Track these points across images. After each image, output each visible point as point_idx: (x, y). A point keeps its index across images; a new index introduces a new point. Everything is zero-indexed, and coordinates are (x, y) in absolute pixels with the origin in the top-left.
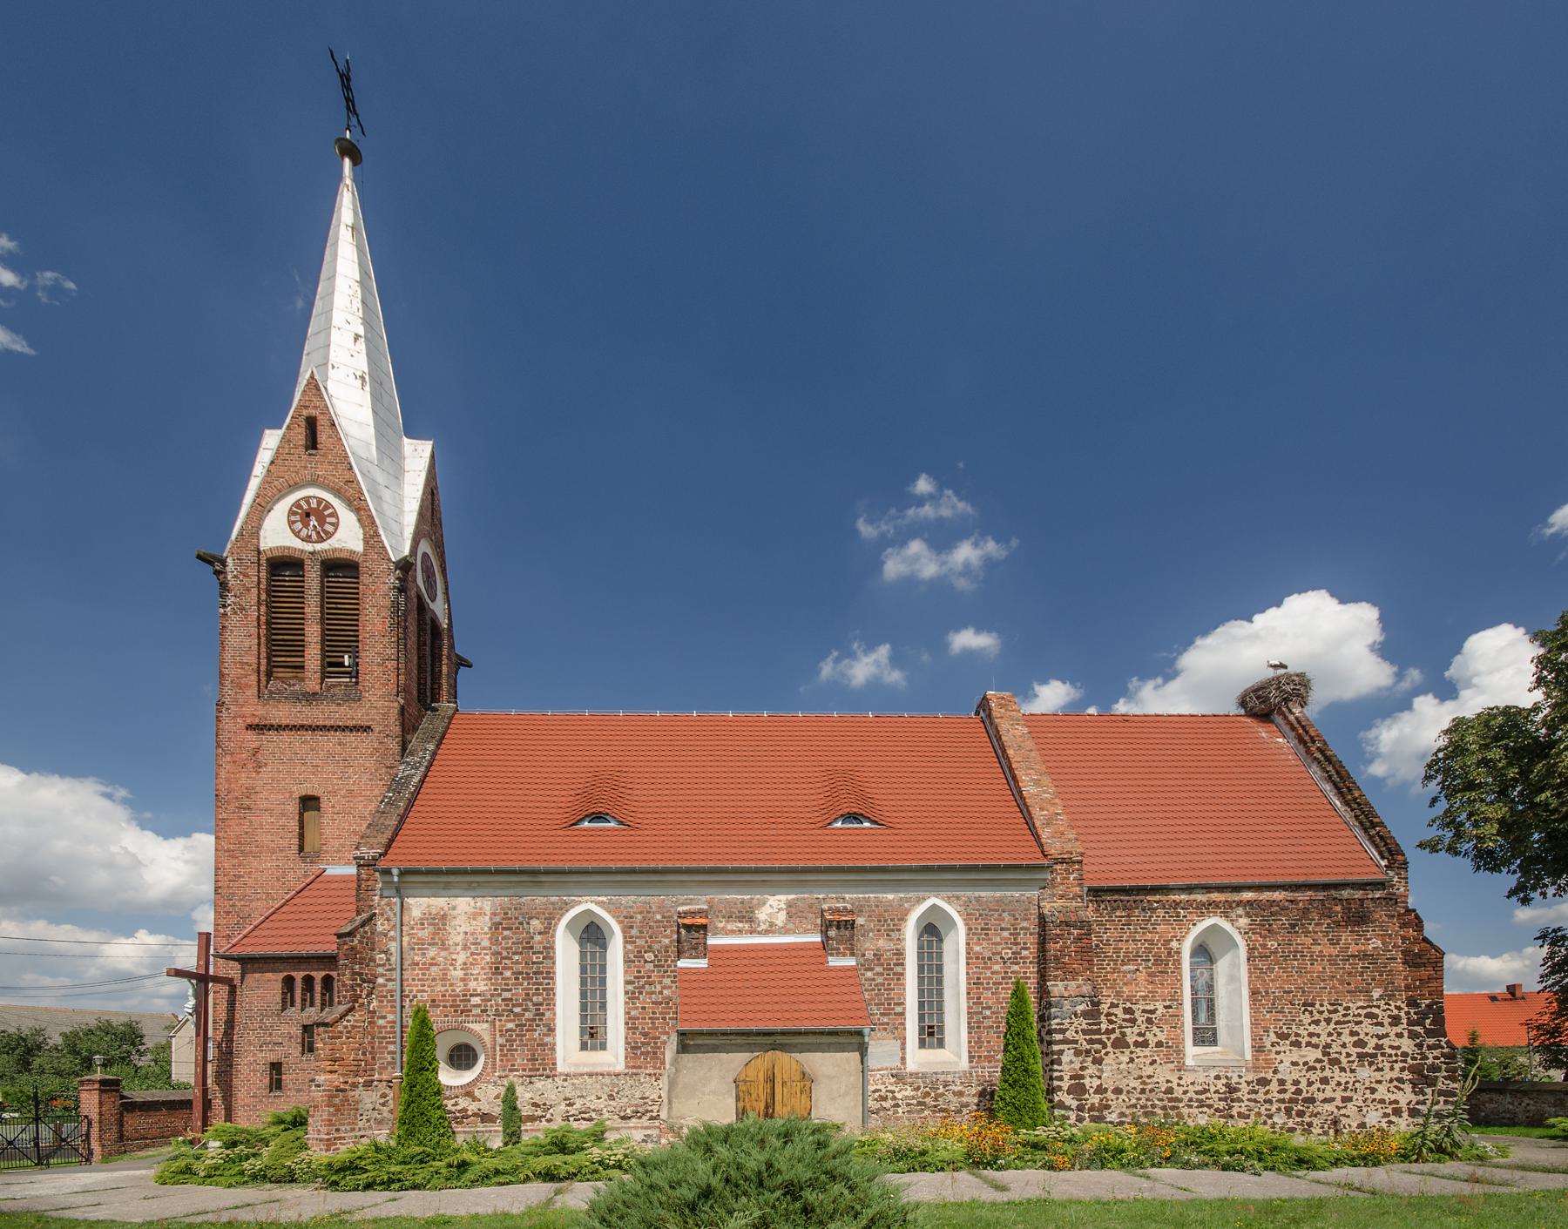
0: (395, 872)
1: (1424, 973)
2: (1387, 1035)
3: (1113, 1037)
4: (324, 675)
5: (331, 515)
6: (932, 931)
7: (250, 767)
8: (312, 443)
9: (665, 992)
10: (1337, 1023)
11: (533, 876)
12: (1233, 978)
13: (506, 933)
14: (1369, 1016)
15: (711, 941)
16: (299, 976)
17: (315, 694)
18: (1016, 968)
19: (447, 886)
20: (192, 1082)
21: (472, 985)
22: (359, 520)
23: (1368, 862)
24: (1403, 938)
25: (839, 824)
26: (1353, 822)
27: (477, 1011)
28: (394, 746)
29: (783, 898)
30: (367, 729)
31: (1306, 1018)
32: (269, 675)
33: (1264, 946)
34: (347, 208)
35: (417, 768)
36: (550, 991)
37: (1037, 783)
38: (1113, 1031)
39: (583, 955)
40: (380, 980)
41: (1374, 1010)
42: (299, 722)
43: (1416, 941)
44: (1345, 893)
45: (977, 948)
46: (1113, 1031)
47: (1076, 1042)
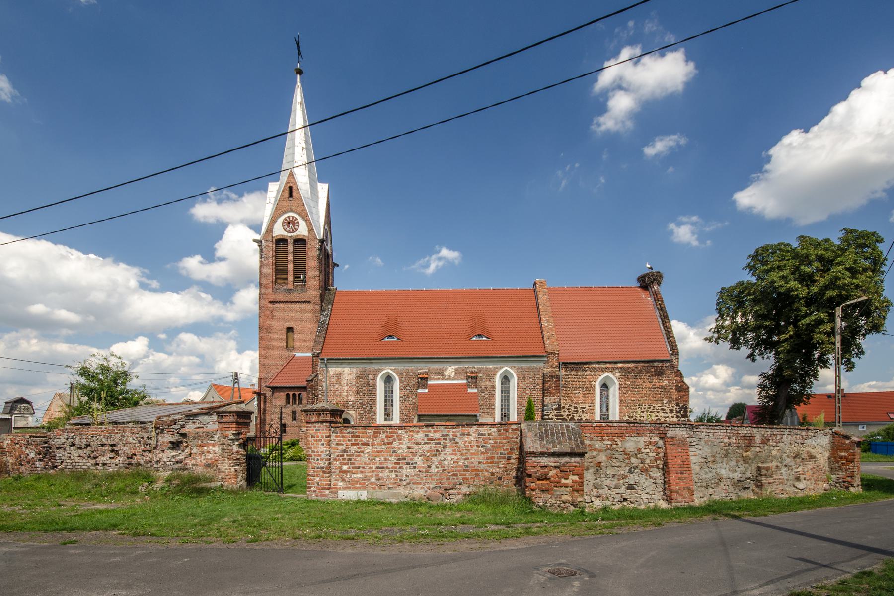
0: (326, 359)
1: (682, 394)
2: (668, 417)
3: (570, 417)
4: (295, 281)
5: (297, 222)
6: (506, 379)
7: (270, 317)
8: (291, 195)
9: (413, 401)
10: (650, 412)
11: (370, 360)
12: (614, 396)
13: (361, 380)
14: (662, 409)
15: (429, 383)
16: (291, 394)
17: (291, 289)
18: (534, 392)
19: (342, 363)
20: (768, 491)
21: (349, 398)
22: (307, 224)
23: (667, 353)
24: (676, 381)
25: (474, 339)
26: (665, 335)
27: (351, 407)
28: (318, 308)
29: (454, 367)
30: (309, 302)
31: (639, 410)
32: (275, 282)
33: (625, 384)
34: (298, 96)
35: (327, 317)
36: (375, 400)
37: (548, 321)
38: (570, 415)
39: (385, 387)
40: (320, 396)
41: (664, 408)
42: (286, 300)
43: (680, 382)
44: (656, 364)
45: (521, 385)
46: (570, 415)
47: (552, 419)
